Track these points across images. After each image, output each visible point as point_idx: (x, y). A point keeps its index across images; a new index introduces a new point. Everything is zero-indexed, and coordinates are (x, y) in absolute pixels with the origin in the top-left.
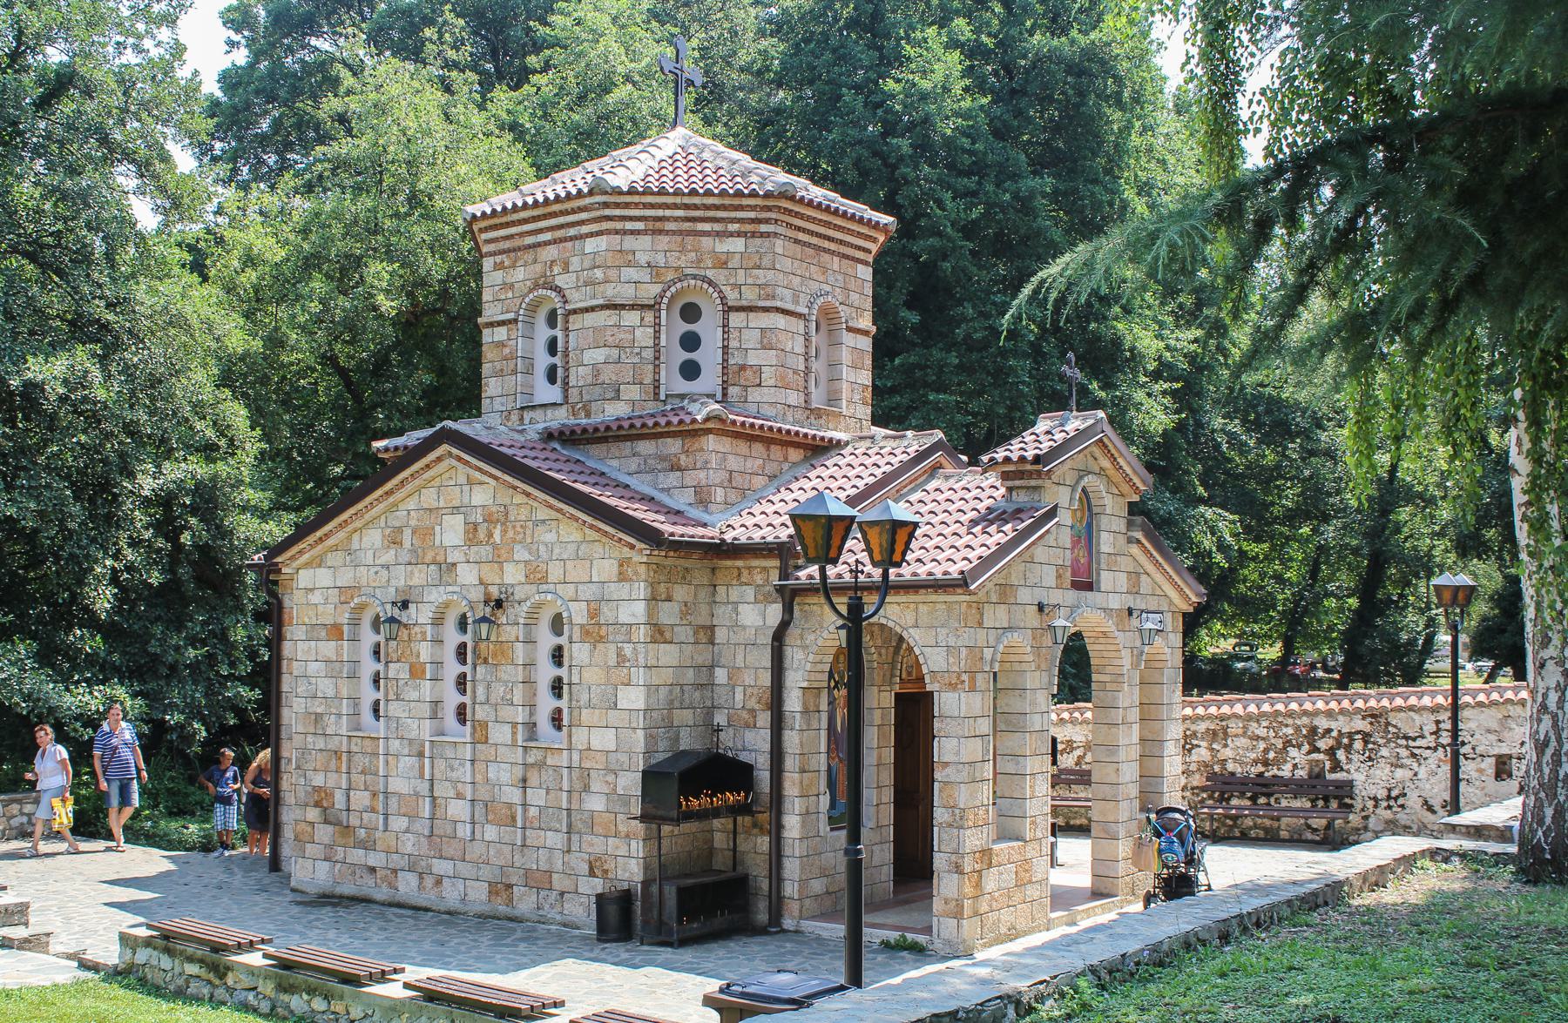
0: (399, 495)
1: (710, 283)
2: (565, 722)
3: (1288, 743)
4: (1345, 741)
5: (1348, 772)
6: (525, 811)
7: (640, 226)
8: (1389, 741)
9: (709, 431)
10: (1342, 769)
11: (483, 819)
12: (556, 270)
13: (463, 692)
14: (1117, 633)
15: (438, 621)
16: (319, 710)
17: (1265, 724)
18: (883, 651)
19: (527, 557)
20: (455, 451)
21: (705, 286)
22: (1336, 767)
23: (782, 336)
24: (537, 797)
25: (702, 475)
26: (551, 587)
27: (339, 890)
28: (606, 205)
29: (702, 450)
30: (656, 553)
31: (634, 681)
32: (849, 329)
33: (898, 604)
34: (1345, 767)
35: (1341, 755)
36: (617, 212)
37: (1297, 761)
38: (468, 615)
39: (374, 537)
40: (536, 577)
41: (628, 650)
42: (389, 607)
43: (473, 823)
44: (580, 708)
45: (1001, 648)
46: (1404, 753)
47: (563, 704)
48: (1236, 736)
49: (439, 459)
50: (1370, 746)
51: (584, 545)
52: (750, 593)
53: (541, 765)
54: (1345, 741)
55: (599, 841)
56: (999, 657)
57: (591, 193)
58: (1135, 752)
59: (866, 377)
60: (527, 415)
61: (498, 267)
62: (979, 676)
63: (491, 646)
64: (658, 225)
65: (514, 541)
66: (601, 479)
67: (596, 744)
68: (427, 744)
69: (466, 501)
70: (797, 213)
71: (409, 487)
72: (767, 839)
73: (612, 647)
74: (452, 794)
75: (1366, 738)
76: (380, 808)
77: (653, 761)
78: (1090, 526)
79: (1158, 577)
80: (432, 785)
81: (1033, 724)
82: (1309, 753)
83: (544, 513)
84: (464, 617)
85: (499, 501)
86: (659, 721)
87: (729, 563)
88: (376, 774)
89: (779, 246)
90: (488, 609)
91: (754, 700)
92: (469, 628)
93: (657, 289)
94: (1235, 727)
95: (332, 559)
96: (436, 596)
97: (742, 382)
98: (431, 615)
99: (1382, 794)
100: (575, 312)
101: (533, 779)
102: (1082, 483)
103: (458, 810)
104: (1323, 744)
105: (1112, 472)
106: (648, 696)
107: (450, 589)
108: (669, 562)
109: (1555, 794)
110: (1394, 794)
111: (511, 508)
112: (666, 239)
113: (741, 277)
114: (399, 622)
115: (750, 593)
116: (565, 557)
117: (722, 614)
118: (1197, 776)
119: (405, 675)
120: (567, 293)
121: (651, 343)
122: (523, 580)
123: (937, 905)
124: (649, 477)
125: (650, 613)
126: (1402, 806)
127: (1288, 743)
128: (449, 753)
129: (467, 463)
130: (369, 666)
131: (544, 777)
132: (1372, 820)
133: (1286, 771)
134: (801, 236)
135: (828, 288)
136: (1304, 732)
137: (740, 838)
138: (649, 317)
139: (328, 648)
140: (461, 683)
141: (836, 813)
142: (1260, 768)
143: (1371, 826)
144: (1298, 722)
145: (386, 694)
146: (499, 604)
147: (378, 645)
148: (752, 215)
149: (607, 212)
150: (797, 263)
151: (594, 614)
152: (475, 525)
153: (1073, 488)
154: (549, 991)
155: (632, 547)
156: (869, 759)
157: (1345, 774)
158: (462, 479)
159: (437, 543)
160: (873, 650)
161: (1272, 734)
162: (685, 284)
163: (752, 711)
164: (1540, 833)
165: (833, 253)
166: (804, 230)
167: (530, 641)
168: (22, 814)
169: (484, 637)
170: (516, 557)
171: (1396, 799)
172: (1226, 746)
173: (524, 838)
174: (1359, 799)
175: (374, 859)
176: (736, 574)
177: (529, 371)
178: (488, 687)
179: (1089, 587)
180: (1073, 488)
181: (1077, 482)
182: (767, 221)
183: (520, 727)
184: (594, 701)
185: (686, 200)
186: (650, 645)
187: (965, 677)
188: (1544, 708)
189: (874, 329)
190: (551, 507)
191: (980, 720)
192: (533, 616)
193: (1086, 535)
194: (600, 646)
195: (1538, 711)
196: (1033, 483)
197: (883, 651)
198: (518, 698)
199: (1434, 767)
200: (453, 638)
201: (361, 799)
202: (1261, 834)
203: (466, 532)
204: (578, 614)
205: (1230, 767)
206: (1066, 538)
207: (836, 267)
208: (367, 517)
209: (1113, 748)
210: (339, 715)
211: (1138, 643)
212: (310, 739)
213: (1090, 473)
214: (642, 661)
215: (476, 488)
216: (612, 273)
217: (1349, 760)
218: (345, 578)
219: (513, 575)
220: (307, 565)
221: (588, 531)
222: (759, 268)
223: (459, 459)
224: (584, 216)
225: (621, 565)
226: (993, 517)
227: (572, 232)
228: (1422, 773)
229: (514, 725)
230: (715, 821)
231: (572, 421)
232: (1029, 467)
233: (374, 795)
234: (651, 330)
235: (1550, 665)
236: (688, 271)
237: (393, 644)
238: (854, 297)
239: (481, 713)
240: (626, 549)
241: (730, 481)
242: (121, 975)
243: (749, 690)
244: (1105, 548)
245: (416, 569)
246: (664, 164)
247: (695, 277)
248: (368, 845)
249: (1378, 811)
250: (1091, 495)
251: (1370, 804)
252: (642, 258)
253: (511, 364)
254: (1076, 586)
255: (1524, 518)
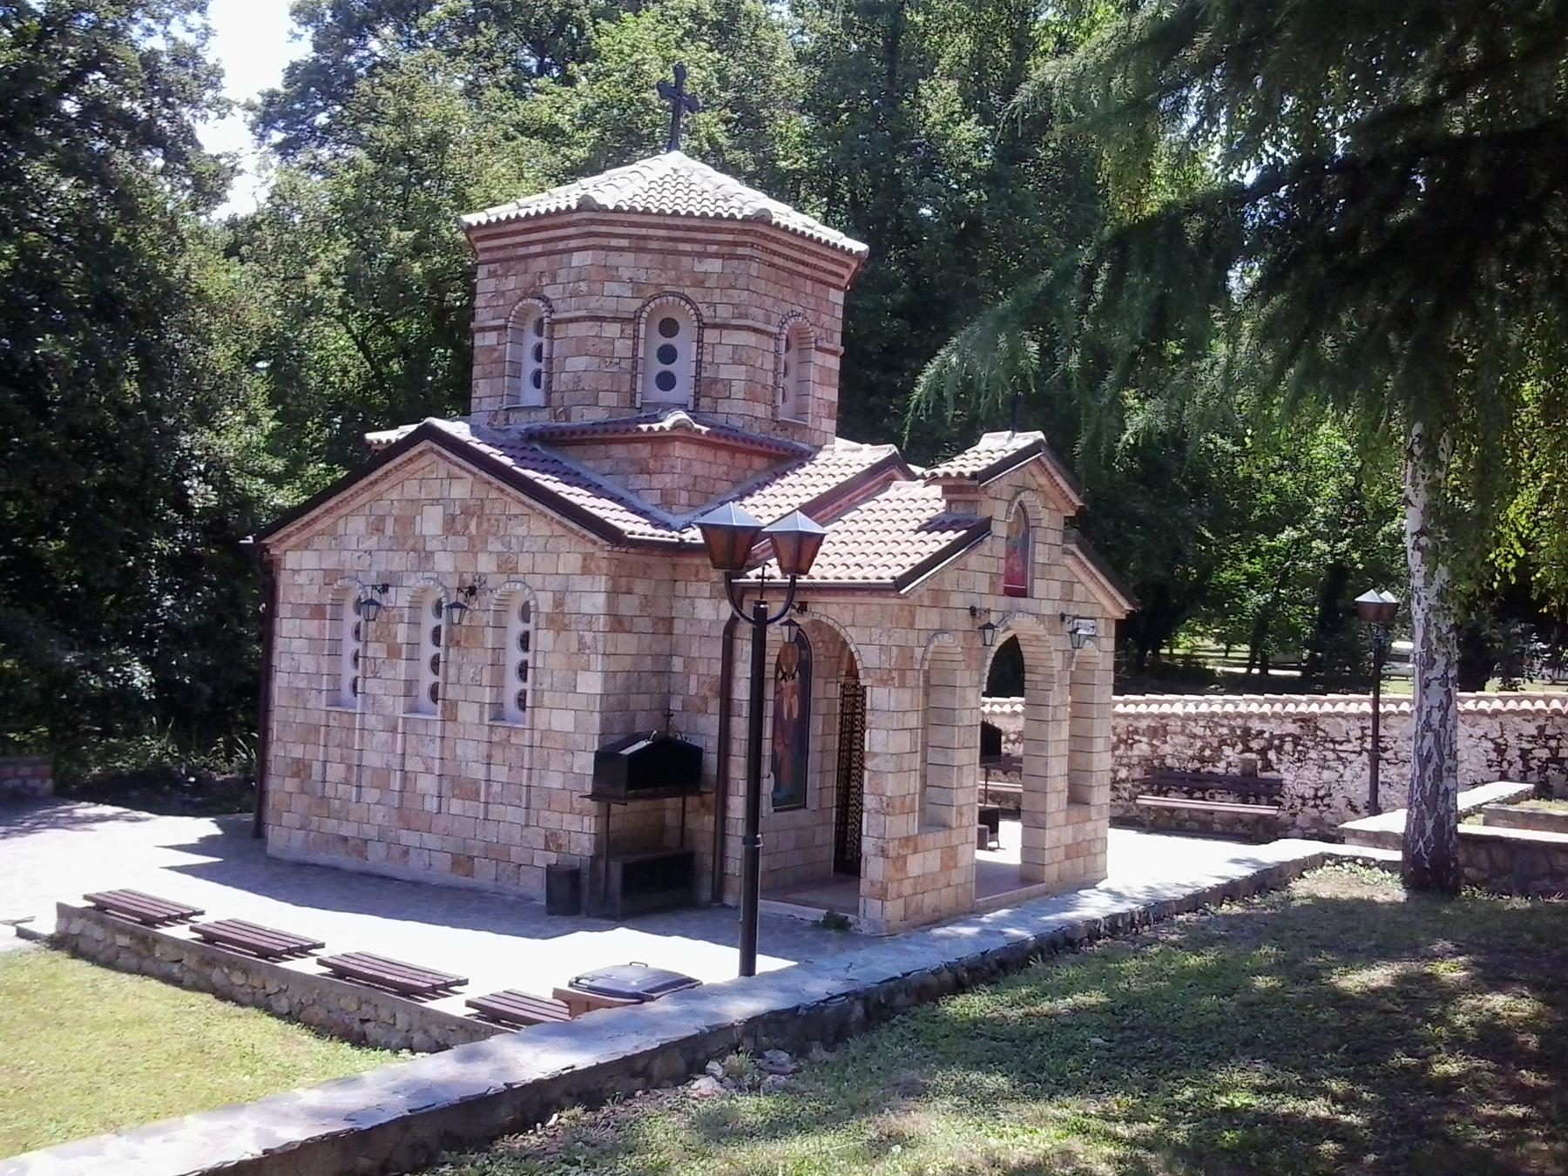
0: (383, 486)
1: (688, 301)
2: (529, 703)
3: (1223, 742)
4: (1276, 742)
5: (1278, 771)
6: (488, 787)
7: (624, 243)
8: (1317, 744)
9: (675, 439)
10: (1273, 769)
11: (450, 793)
12: (545, 281)
13: (436, 672)
14: (1048, 637)
15: (415, 606)
16: (301, 685)
17: (1201, 723)
18: (831, 646)
19: (499, 548)
20: (436, 447)
21: (683, 303)
22: (1268, 766)
23: (753, 354)
24: (500, 774)
25: (668, 478)
26: (520, 577)
27: (311, 859)
28: (593, 222)
29: (669, 456)
30: (617, 549)
31: (593, 667)
32: (818, 349)
33: (838, 604)
34: (1276, 767)
35: (1272, 755)
36: (603, 229)
37: (1231, 759)
38: (443, 600)
39: (357, 525)
40: (507, 567)
41: (588, 637)
42: (369, 589)
43: (440, 797)
44: (543, 691)
45: (931, 648)
46: (1330, 755)
47: (528, 686)
48: (1175, 733)
49: (421, 454)
50: (1300, 748)
51: (551, 541)
52: (706, 589)
53: (505, 744)
54: (1276, 742)
55: (554, 816)
56: (929, 656)
57: (579, 209)
58: (1064, 748)
59: (832, 395)
60: (513, 417)
61: (491, 274)
62: (909, 673)
63: (464, 630)
64: (641, 243)
65: (488, 532)
66: (571, 478)
67: (556, 726)
68: (400, 720)
69: (445, 494)
70: (773, 238)
71: (393, 479)
72: (713, 818)
73: (574, 636)
74: (421, 768)
75: (1296, 740)
76: (354, 779)
77: (608, 743)
78: (1026, 537)
79: (1092, 586)
80: (404, 759)
81: (961, 719)
82: (1242, 752)
83: (515, 509)
84: (439, 602)
85: (476, 495)
86: (615, 707)
87: (687, 560)
88: (352, 748)
89: (754, 268)
90: (461, 596)
91: (706, 687)
92: (444, 611)
93: (638, 303)
94: (1174, 726)
95: (319, 543)
96: (414, 582)
97: (713, 394)
98: (409, 599)
99: (1309, 793)
100: (559, 321)
101: (498, 755)
102: (1018, 499)
103: (427, 784)
104: (1254, 745)
105: (1048, 489)
106: (605, 682)
107: (427, 575)
108: (630, 558)
109: (1436, 807)
110: (1321, 793)
111: (487, 502)
112: (649, 257)
113: (717, 296)
114: (378, 605)
115: (706, 589)
116: (534, 549)
117: (681, 607)
118: (1138, 769)
119: (382, 655)
120: (554, 303)
121: (630, 355)
122: (495, 569)
123: (864, 886)
124: (620, 479)
125: (611, 603)
126: (1329, 806)
127: (1223, 742)
128: (421, 729)
129: (446, 458)
130: (350, 646)
131: (507, 755)
132: (1299, 817)
133: (1220, 768)
134: (776, 260)
135: (800, 310)
136: (1238, 732)
137: (689, 818)
138: (629, 330)
139: (312, 627)
140: (435, 663)
141: (779, 795)
142: (1197, 765)
143: (1298, 823)
144: (1233, 723)
145: (365, 672)
146: (472, 591)
147: (358, 625)
148: (730, 238)
149: (594, 228)
150: (770, 285)
151: (559, 603)
152: (453, 518)
153: (1010, 503)
154: (449, 968)
155: (595, 543)
156: (814, 745)
157: (1275, 773)
158: (443, 474)
159: (417, 532)
160: (820, 644)
161: (1208, 732)
162: (664, 300)
163: (705, 699)
164: (1421, 843)
165: (806, 277)
166: (779, 255)
167: (500, 627)
168: (17, 777)
169: (456, 621)
170: (490, 548)
171: (1322, 798)
172: (1165, 742)
173: (486, 812)
174: (1288, 797)
175: (348, 830)
176: (694, 571)
177: (516, 375)
178: (460, 668)
179: (1023, 594)
180: (1010, 503)
181: (1014, 498)
182: (744, 244)
183: (487, 706)
184: (555, 685)
185: (669, 221)
186: (609, 635)
187: (895, 674)
188: (1427, 725)
189: (842, 350)
190: (523, 503)
191: (908, 715)
192: (503, 603)
193: (1020, 546)
194: (563, 634)
195: (1422, 728)
196: (970, 497)
197: (831, 646)
198: (486, 678)
199: (1358, 770)
200: (430, 622)
201: (336, 771)
202: (1196, 825)
203: (445, 523)
204: (545, 603)
205: (1169, 762)
206: (1000, 548)
207: (809, 290)
208: (353, 505)
209: (1042, 743)
210: (320, 691)
211: (1069, 647)
212: (291, 712)
213: (1028, 489)
214: (600, 649)
215: (455, 482)
216: (597, 286)
217: (1280, 760)
218: (330, 562)
219: (486, 564)
220: (295, 548)
221: (556, 526)
222: (734, 288)
223: (440, 455)
224: (572, 231)
225: (585, 559)
226: (933, 526)
227: (561, 245)
228: (1348, 775)
229: (482, 704)
230: (667, 800)
231: (553, 423)
232: (967, 483)
233: (349, 767)
234: (630, 342)
235: (1435, 685)
236: (667, 288)
237: (372, 625)
238: (825, 318)
239: (452, 692)
240: (589, 545)
241: (694, 485)
242: (57, 942)
243: (702, 678)
244: (1040, 559)
245: (397, 556)
246: (653, 185)
247: (673, 294)
248: (343, 817)
249: (1306, 809)
250: (1028, 509)
251: (1298, 802)
252: (625, 274)
253: (500, 367)
254: (1010, 593)
255: (1417, 547)
